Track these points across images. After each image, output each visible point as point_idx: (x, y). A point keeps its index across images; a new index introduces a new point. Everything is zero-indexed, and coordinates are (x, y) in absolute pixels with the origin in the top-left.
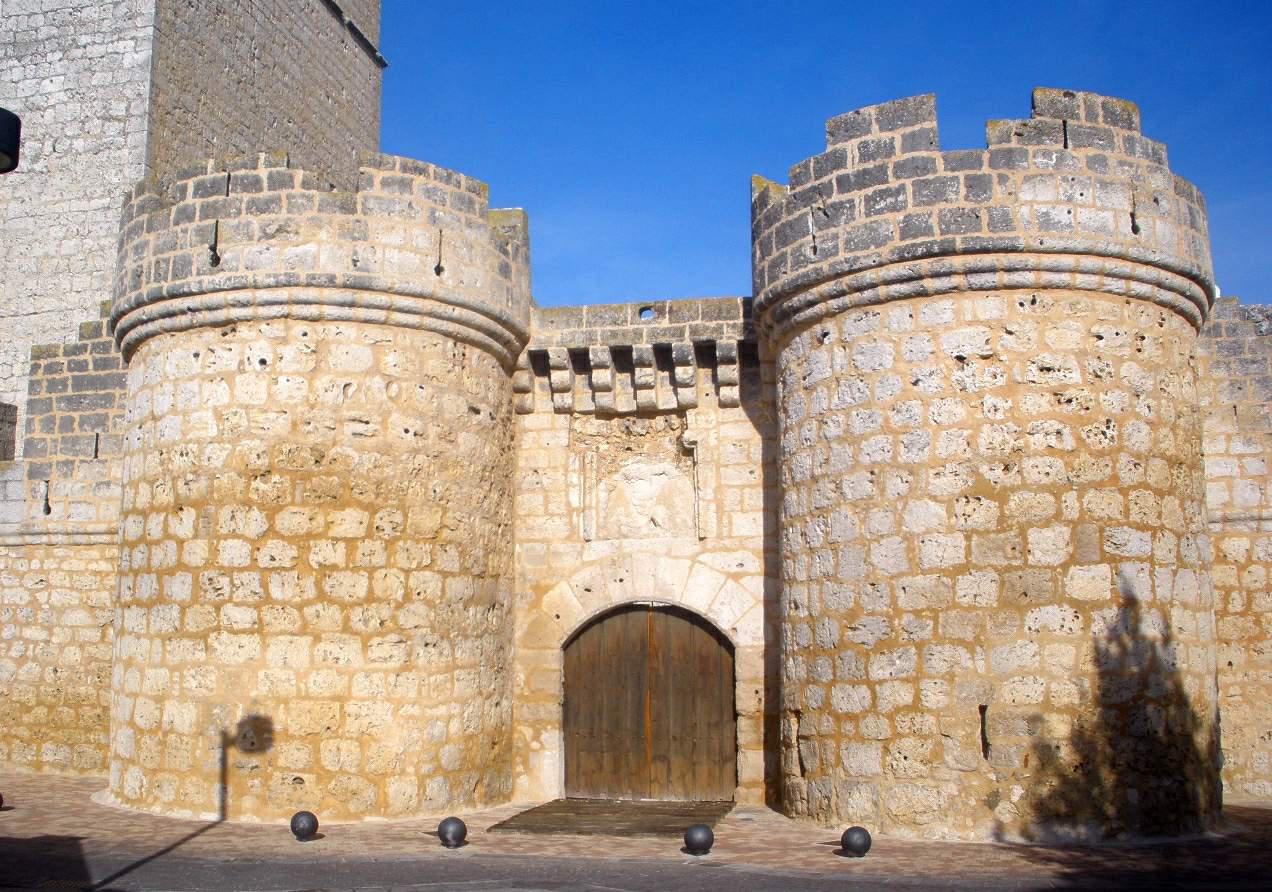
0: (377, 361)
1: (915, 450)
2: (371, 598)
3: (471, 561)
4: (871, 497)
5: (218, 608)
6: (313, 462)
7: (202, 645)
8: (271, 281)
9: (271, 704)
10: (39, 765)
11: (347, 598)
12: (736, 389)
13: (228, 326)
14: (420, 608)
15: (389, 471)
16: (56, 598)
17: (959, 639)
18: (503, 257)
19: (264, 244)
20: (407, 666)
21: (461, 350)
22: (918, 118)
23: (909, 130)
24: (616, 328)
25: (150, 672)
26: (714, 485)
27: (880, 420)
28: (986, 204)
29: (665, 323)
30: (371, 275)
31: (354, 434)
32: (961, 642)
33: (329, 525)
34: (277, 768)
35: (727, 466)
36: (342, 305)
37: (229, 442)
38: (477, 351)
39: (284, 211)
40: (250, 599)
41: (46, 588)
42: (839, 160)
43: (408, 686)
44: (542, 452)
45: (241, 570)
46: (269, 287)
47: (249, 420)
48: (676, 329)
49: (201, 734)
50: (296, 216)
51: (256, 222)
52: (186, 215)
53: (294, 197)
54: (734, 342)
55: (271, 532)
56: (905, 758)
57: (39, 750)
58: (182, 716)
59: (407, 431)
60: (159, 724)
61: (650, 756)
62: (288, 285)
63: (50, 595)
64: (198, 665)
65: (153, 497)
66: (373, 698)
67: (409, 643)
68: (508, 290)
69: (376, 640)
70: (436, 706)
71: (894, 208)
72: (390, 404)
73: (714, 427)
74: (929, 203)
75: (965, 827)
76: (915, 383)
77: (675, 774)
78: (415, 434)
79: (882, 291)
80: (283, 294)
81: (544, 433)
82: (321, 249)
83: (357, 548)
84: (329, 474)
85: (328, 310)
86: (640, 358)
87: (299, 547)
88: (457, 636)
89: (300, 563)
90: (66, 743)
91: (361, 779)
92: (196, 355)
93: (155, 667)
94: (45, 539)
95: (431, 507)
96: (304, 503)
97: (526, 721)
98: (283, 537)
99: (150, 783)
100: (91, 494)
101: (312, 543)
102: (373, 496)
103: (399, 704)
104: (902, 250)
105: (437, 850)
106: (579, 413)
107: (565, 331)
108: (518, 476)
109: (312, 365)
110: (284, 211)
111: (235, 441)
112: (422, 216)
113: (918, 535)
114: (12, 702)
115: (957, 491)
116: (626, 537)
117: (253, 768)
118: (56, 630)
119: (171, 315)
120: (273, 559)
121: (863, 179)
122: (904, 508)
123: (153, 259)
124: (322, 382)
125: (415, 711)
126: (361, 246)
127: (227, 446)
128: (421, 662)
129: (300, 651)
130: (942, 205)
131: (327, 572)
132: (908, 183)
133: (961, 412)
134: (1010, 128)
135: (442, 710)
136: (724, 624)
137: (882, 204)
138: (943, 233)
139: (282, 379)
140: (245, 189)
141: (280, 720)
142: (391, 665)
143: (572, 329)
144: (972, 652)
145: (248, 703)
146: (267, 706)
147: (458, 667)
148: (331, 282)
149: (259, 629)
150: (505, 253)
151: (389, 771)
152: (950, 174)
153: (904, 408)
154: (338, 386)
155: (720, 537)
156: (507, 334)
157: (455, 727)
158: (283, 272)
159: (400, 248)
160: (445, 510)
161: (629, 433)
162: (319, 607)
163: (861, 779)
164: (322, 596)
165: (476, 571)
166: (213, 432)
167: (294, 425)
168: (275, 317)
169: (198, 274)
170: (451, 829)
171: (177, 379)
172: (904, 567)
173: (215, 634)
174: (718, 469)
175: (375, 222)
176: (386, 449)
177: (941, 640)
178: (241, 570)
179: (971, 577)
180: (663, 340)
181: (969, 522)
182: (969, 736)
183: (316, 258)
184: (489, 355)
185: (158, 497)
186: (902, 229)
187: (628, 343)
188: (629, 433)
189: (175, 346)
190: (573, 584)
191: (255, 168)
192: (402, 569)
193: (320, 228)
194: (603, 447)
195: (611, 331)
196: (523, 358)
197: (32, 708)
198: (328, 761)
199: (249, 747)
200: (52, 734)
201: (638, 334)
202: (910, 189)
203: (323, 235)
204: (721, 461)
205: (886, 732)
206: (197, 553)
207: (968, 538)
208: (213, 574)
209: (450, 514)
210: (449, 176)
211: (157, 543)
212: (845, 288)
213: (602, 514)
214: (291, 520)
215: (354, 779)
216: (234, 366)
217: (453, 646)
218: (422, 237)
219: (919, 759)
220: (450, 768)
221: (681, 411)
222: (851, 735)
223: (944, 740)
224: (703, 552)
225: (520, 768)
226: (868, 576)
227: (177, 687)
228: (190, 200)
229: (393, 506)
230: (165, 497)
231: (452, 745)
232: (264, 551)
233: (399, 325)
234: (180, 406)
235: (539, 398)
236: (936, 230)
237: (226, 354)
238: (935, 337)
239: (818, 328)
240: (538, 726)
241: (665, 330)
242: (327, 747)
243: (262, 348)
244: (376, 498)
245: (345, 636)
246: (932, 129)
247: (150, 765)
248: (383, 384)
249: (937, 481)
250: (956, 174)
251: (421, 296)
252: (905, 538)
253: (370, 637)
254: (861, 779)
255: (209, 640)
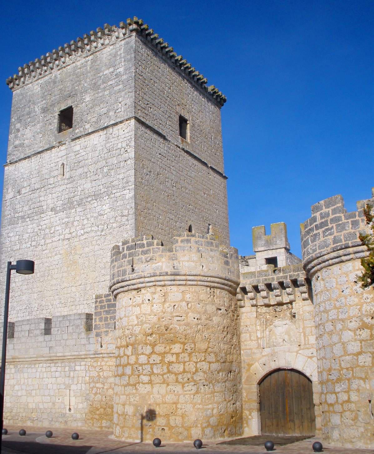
0: (184, 297)
1: (343, 314)
2: (184, 371)
3: (220, 358)
4: (332, 331)
5: (139, 376)
6: (165, 330)
7: (135, 388)
8: (149, 275)
9: (155, 405)
10: (101, 427)
11: (177, 372)
12: (307, 294)
13: (138, 289)
14: (201, 374)
15: (189, 331)
16: (105, 374)
17: (360, 377)
18: (225, 259)
19: (146, 264)
20: (197, 392)
21: (213, 290)
22: (336, 203)
23: (333, 207)
24: (266, 277)
25: (121, 397)
26: (302, 327)
27: (333, 305)
28: (358, 230)
29: (281, 274)
30: (179, 271)
31: (177, 321)
32: (361, 378)
33: (171, 349)
34: (156, 425)
35: (306, 320)
36: (171, 281)
37: (140, 325)
38: (219, 290)
39: (152, 253)
40: (148, 373)
41: (102, 371)
42: (314, 219)
43: (198, 399)
44: (248, 320)
45: (145, 364)
46: (148, 277)
47: (146, 318)
48: (285, 276)
49: (135, 415)
50: (155, 254)
51: (143, 257)
52: (125, 256)
53: (154, 249)
54: (303, 279)
55: (153, 352)
56: (347, 419)
57: (101, 422)
58: (130, 410)
59: (194, 318)
60: (124, 412)
61: (288, 420)
62: (154, 276)
63: (103, 373)
64: (133, 394)
65: (121, 343)
66: (186, 402)
67: (198, 385)
68: (228, 269)
69: (186, 385)
70: (208, 405)
71: (330, 234)
72: (189, 310)
73: (302, 308)
74: (340, 232)
75: (367, 444)
76: (343, 292)
77: (296, 427)
78: (197, 319)
79: (331, 262)
80: (153, 279)
81: (248, 314)
82: (163, 264)
83: (179, 356)
84: (170, 333)
85: (167, 283)
86: (274, 286)
87: (162, 357)
88: (215, 382)
89: (162, 361)
90: (109, 420)
91: (183, 429)
92: (130, 299)
93: (123, 395)
94: (101, 355)
95: (204, 342)
96: (163, 343)
97: (247, 409)
98: (157, 354)
99: (122, 431)
100: (114, 341)
101: (165, 355)
102: (184, 340)
103: (194, 405)
104: (333, 248)
105: (194, 450)
106: (260, 306)
107: (251, 280)
108: (241, 328)
109: (163, 300)
110: (152, 253)
111: (142, 325)
112: (195, 250)
113: (346, 343)
114: (93, 407)
115: (357, 327)
116: (276, 346)
117: (150, 426)
118: (106, 384)
119: (123, 287)
120: (154, 361)
121: (322, 225)
122: (342, 333)
123: (117, 270)
124: (167, 305)
125: (201, 406)
126: (175, 262)
127: (140, 326)
128: (202, 391)
129: (163, 389)
130: (345, 232)
131: (171, 364)
132: (334, 225)
133: (356, 300)
134: (364, 203)
135: (210, 406)
136: (308, 374)
137: (327, 233)
138: (345, 241)
139: (155, 305)
140: (140, 248)
141: (158, 410)
142: (192, 392)
143: (253, 279)
144: (365, 382)
145: (148, 406)
146: (153, 406)
147: (216, 392)
148: (167, 274)
149: (150, 382)
150: (227, 257)
151: (192, 426)
152: (346, 221)
153: (340, 300)
154: (172, 306)
155: (305, 344)
156: (230, 283)
157: (215, 411)
158: (152, 272)
159: (188, 261)
160: (209, 342)
161: (276, 311)
162: (168, 375)
163: (336, 426)
164: (169, 372)
165: (222, 361)
166: (136, 322)
167: (159, 319)
168: (151, 286)
169: (129, 275)
170: (197, 443)
171: (126, 307)
172: (343, 354)
173: (138, 384)
174: (303, 322)
175: (179, 254)
176: (187, 325)
177: (354, 378)
178: (145, 364)
179: (362, 356)
180: (281, 280)
181: (361, 337)
182: (366, 411)
183: (162, 267)
184: (224, 291)
185: (122, 343)
186: (333, 241)
187: (270, 282)
188: (276, 311)
189: (125, 296)
190: (260, 363)
191: (143, 241)
192: (195, 362)
193: (163, 258)
194: (268, 317)
195: (265, 279)
196: (238, 290)
197: (99, 409)
198: (172, 423)
199: (148, 419)
200: (105, 417)
201: (273, 279)
202: (335, 227)
203: (163, 260)
204: (304, 319)
205: (341, 410)
206: (133, 359)
207: (361, 343)
208: (137, 366)
209: (211, 343)
210: (203, 236)
211: (122, 357)
212: (320, 262)
213: (268, 339)
214: (159, 348)
215: (180, 429)
216: (141, 302)
217: (213, 385)
218: (195, 256)
219: (351, 419)
220: (214, 425)
221: (291, 303)
222: (332, 411)
223: (358, 412)
224: (299, 350)
225: (245, 425)
226: (333, 357)
227: (128, 401)
228: (125, 252)
229: (191, 342)
230: (124, 343)
231: (214, 417)
232: (151, 358)
233: (190, 285)
234: (127, 315)
235: (247, 303)
236: (343, 240)
237: (139, 298)
238: (347, 276)
239: (316, 275)
240: (250, 410)
241: (281, 277)
242: (172, 418)
243: (148, 296)
244: (185, 340)
245: (176, 384)
246: (340, 207)
247: (121, 425)
248: (186, 304)
249: (350, 324)
250: (348, 220)
251: (196, 275)
252: (343, 344)
253: (185, 383)
254: (336, 426)
255: (137, 386)
